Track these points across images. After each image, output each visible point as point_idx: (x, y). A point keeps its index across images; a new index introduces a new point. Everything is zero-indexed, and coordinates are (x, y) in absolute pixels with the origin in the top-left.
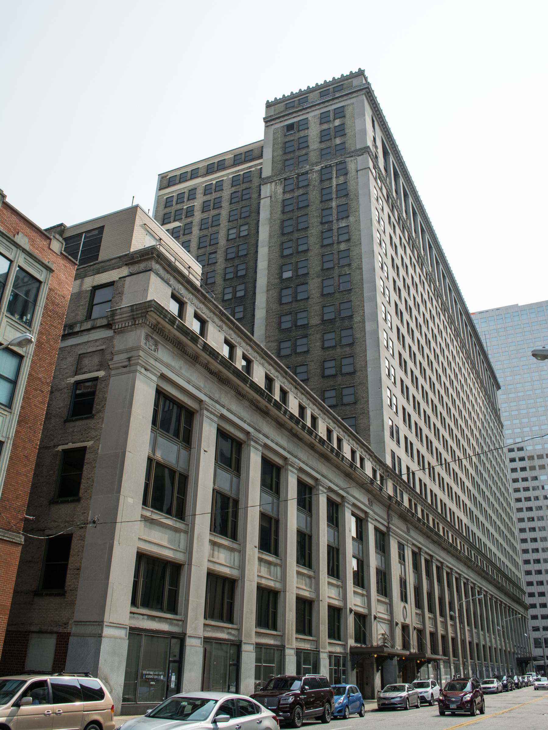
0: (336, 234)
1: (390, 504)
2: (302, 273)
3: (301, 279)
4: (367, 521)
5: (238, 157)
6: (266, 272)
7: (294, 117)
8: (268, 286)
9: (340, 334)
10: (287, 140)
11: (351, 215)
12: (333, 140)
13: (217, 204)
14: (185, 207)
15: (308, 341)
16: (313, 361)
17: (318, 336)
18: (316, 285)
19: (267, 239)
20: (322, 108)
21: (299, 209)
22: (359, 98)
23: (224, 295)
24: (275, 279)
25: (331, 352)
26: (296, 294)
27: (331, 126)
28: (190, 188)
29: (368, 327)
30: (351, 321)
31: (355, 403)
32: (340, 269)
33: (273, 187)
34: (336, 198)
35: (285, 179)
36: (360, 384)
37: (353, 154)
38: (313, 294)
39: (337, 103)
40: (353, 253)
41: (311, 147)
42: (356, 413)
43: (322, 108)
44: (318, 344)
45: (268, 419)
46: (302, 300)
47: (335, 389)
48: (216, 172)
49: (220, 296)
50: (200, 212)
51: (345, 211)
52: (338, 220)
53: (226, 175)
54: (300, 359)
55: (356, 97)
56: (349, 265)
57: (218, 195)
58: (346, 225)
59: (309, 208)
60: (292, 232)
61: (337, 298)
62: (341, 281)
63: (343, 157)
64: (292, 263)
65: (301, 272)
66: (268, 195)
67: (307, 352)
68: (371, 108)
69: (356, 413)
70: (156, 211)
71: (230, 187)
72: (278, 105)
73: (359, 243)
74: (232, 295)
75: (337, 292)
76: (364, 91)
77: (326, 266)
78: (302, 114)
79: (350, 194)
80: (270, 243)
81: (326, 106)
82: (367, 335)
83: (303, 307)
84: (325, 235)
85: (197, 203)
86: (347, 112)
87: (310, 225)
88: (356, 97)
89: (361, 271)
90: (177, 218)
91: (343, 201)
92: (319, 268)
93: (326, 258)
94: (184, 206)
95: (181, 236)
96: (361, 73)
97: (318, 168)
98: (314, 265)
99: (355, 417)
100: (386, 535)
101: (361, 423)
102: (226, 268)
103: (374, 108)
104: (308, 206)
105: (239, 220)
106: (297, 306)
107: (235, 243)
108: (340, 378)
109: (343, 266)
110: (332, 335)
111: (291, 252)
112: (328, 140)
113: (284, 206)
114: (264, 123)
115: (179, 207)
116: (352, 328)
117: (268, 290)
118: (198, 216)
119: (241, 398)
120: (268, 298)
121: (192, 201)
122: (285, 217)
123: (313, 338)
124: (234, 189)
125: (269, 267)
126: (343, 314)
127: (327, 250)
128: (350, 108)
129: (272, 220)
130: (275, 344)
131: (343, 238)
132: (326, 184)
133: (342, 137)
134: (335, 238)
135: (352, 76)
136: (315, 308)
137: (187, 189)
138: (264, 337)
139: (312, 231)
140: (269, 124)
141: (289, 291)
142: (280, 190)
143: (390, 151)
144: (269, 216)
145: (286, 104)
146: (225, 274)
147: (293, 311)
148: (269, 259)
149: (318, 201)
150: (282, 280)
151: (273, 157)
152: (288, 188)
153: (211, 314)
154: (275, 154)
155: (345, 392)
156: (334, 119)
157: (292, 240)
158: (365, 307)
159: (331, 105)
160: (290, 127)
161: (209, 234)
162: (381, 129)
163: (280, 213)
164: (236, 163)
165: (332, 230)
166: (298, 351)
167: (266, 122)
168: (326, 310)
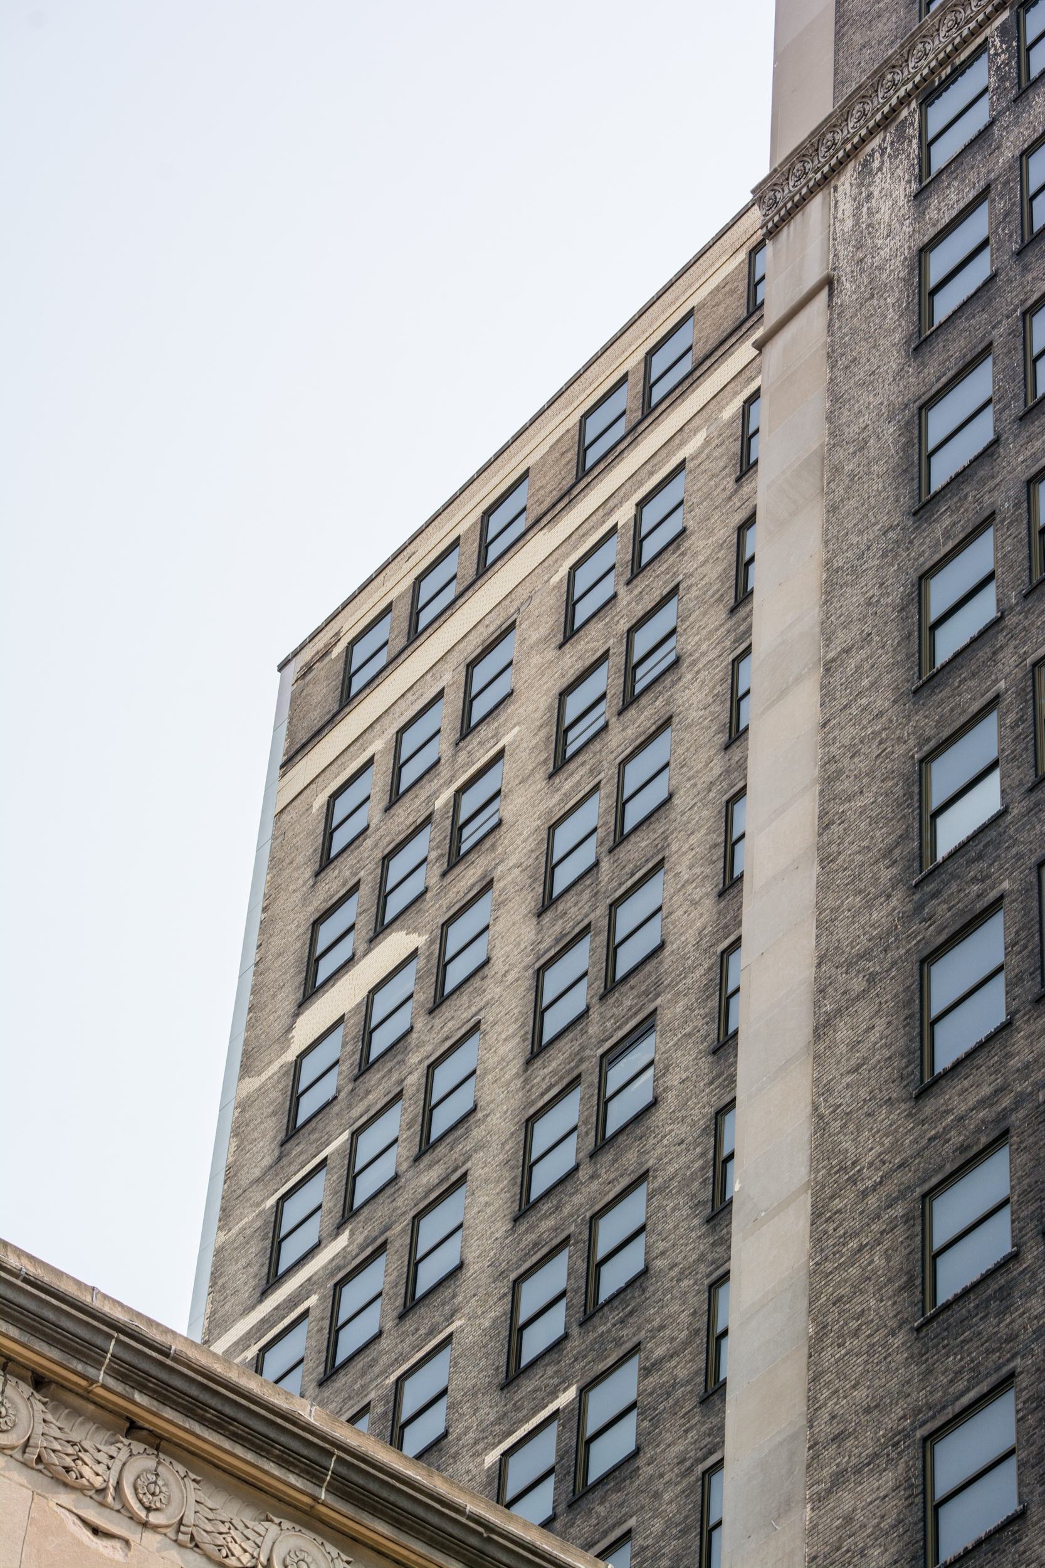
33: (846, 206)
66: (813, 276)
70: (264, 926)
71: (729, 482)
80: (828, 641)
94: (430, 799)
117: (821, 1029)
120: (823, 1089)
121: (484, 732)
130: (888, 1479)
138: (804, 1455)
161: (602, 910)
163: (894, 360)
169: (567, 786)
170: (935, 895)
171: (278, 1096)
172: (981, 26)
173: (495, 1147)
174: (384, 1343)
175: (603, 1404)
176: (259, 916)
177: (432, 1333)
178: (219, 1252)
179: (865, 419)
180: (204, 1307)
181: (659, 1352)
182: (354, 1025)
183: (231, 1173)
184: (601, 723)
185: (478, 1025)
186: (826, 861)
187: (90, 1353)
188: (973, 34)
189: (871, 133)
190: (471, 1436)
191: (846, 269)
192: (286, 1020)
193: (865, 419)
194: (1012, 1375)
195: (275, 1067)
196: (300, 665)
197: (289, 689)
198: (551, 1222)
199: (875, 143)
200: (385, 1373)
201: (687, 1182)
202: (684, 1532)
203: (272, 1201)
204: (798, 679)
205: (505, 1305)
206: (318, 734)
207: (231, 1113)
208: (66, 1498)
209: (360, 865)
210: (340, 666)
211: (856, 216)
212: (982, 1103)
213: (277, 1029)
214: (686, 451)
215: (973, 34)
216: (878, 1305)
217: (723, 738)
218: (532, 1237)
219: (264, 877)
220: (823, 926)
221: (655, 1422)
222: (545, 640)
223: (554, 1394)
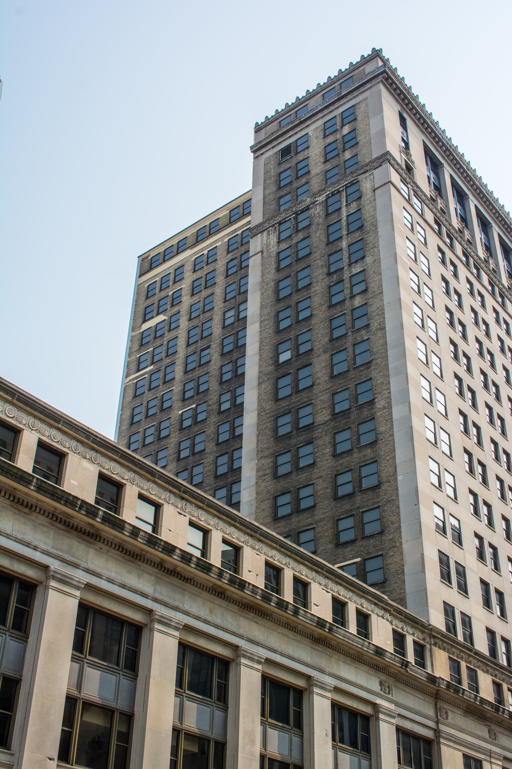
0: (349, 285)
1: (438, 690)
2: (304, 351)
3: (303, 360)
4: (378, 719)
5: (235, 212)
6: (257, 358)
7: (290, 137)
8: (259, 378)
9: (358, 431)
10: (282, 170)
11: (367, 254)
12: (341, 156)
13: (209, 283)
14: (171, 293)
15: (314, 449)
16: (321, 477)
17: (327, 439)
18: (323, 364)
19: (258, 312)
20: (326, 115)
21: (298, 260)
22: (374, 89)
23: (220, 405)
24: (268, 366)
25: (345, 460)
26: (296, 381)
27: (338, 136)
28: (176, 267)
29: (397, 413)
30: (372, 409)
31: (381, 533)
32: (355, 335)
33: (265, 238)
34: (347, 234)
35: (280, 223)
36: (388, 501)
37: (368, 168)
38: (319, 378)
39: (344, 103)
40: (372, 309)
41: (313, 173)
42: (383, 549)
43: (326, 115)
44: (328, 450)
45: (100, 545)
46: (304, 389)
47: (353, 515)
48: (207, 238)
49: (215, 407)
50: (189, 296)
51: (360, 250)
52: (350, 265)
53: (219, 239)
54: (302, 477)
55: (369, 88)
56: (367, 326)
57: (210, 268)
58: (362, 269)
59: (312, 257)
60: (290, 295)
61: (352, 379)
62: (357, 352)
63: (355, 175)
64: (290, 339)
65: (303, 349)
66: (259, 250)
67: (312, 465)
68: (397, 101)
69: (383, 549)
70: (136, 305)
71: (225, 254)
72: (270, 126)
73: (379, 291)
74: (231, 404)
75: (351, 369)
76: (380, 78)
77: (336, 334)
78: (301, 130)
79: (365, 224)
80: (261, 317)
81: (331, 112)
82: (394, 426)
83: (305, 400)
84: (334, 290)
85: (185, 285)
86: (358, 113)
87: (314, 280)
88: (369, 88)
89: (383, 332)
90: (161, 309)
91: (357, 236)
92: (327, 339)
93: (335, 323)
94: (168, 292)
95: (166, 333)
96: (376, 54)
97: (322, 198)
98: (319, 335)
99: (382, 555)
100: (435, 744)
101: (390, 564)
102: (222, 366)
103: (403, 100)
104: (310, 253)
105: (237, 296)
106: (297, 399)
107: (232, 329)
108: (359, 498)
109: (359, 330)
110: (346, 435)
111: (290, 324)
112: (335, 156)
113: (279, 261)
114: (252, 154)
115: (163, 294)
116: (373, 419)
117: (259, 384)
118: (186, 301)
119: (26, 510)
120: (260, 394)
121: (179, 283)
122: (280, 275)
123: (320, 442)
124: (230, 256)
125: (260, 350)
126: (362, 400)
127: (337, 311)
128: (363, 107)
129: (264, 284)
130: (270, 460)
131: (357, 289)
132: (333, 218)
133: (354, 148)
134: (347, 292)
135: (365, 61)
136: (322, 398)
137: (173, 268)
138: (256, 452)
139: (317, 288)
140: (258, 153)
141: (287, 380)
142: (273, 239)
143: (443, 161)
144: (259, 279)
145: (280, 122)
146: (222, 375)
147: (293, 407)
148: (261, 338)
149: (323, 245)
150: (278, 365)
151: (264, 198)
152: (284, 236)
153: (74, 443)
154: (267, 193)
155: (368, 517)
156: (343, 126)
157: (290, 306)
158: (392, 385)
159: (338, 108)
160: (286, 152)
161: (200, 324)
162: (421, 131)
163: (273, 271)
164: (232, 219)
165: (343, 280)
166: (301, 465)
167: (254, 152)
168: (338, 398)
169: (194, 299)
170: (280, 368)
171: (139, 337)
172: (290, 216)
173: (181, 360)
174: (160, 387)
175: (200, 409)
176: (135, 303)
177: (169, 388)
178: (128, 362)
179: (268, 279)
180: (126, 371)
181: (210, 403)
182: (153, 329)
183: (130, 348)
184: (200, 290)
185: (177, 337)
186: (260, 356)
187: (256, 532)
188: (289, 216)
189: (270, 227)
190: (176, 408)
191: (265, 250)
192: (140, 324)
193: (268, 279)
194: (290, 450)
195: (138, 332)
196: (143, 259)
197: (140, 262)
198: (191, 376)
199: (270, 229)
200: (161, 392)
201: (216, 376)
202: (214, 434)
203: (138, 356)
204: (256, 322)
205: (182, 387)
206: (146, 273)
207: (130, 338)
208: (254, 551)
209: (155, 299)
210: (150, 261)
211: (267, 241)
212: (287, 406)
213: (139, 325)
214: (218, 244)
215: (289, 216)
216: (269, 433)
217: (223, 300)
218: (187, 377)
219: (136, 296)
220: (260, 367)
221: (210, 415)
222: (190, 270)
223: (191, 405)
